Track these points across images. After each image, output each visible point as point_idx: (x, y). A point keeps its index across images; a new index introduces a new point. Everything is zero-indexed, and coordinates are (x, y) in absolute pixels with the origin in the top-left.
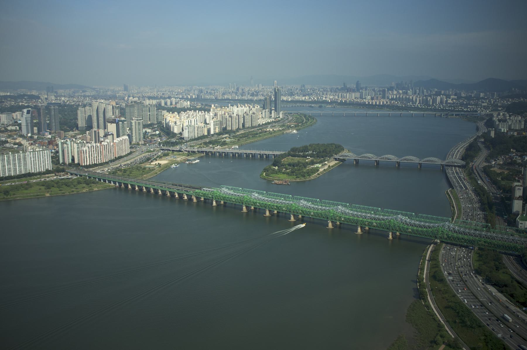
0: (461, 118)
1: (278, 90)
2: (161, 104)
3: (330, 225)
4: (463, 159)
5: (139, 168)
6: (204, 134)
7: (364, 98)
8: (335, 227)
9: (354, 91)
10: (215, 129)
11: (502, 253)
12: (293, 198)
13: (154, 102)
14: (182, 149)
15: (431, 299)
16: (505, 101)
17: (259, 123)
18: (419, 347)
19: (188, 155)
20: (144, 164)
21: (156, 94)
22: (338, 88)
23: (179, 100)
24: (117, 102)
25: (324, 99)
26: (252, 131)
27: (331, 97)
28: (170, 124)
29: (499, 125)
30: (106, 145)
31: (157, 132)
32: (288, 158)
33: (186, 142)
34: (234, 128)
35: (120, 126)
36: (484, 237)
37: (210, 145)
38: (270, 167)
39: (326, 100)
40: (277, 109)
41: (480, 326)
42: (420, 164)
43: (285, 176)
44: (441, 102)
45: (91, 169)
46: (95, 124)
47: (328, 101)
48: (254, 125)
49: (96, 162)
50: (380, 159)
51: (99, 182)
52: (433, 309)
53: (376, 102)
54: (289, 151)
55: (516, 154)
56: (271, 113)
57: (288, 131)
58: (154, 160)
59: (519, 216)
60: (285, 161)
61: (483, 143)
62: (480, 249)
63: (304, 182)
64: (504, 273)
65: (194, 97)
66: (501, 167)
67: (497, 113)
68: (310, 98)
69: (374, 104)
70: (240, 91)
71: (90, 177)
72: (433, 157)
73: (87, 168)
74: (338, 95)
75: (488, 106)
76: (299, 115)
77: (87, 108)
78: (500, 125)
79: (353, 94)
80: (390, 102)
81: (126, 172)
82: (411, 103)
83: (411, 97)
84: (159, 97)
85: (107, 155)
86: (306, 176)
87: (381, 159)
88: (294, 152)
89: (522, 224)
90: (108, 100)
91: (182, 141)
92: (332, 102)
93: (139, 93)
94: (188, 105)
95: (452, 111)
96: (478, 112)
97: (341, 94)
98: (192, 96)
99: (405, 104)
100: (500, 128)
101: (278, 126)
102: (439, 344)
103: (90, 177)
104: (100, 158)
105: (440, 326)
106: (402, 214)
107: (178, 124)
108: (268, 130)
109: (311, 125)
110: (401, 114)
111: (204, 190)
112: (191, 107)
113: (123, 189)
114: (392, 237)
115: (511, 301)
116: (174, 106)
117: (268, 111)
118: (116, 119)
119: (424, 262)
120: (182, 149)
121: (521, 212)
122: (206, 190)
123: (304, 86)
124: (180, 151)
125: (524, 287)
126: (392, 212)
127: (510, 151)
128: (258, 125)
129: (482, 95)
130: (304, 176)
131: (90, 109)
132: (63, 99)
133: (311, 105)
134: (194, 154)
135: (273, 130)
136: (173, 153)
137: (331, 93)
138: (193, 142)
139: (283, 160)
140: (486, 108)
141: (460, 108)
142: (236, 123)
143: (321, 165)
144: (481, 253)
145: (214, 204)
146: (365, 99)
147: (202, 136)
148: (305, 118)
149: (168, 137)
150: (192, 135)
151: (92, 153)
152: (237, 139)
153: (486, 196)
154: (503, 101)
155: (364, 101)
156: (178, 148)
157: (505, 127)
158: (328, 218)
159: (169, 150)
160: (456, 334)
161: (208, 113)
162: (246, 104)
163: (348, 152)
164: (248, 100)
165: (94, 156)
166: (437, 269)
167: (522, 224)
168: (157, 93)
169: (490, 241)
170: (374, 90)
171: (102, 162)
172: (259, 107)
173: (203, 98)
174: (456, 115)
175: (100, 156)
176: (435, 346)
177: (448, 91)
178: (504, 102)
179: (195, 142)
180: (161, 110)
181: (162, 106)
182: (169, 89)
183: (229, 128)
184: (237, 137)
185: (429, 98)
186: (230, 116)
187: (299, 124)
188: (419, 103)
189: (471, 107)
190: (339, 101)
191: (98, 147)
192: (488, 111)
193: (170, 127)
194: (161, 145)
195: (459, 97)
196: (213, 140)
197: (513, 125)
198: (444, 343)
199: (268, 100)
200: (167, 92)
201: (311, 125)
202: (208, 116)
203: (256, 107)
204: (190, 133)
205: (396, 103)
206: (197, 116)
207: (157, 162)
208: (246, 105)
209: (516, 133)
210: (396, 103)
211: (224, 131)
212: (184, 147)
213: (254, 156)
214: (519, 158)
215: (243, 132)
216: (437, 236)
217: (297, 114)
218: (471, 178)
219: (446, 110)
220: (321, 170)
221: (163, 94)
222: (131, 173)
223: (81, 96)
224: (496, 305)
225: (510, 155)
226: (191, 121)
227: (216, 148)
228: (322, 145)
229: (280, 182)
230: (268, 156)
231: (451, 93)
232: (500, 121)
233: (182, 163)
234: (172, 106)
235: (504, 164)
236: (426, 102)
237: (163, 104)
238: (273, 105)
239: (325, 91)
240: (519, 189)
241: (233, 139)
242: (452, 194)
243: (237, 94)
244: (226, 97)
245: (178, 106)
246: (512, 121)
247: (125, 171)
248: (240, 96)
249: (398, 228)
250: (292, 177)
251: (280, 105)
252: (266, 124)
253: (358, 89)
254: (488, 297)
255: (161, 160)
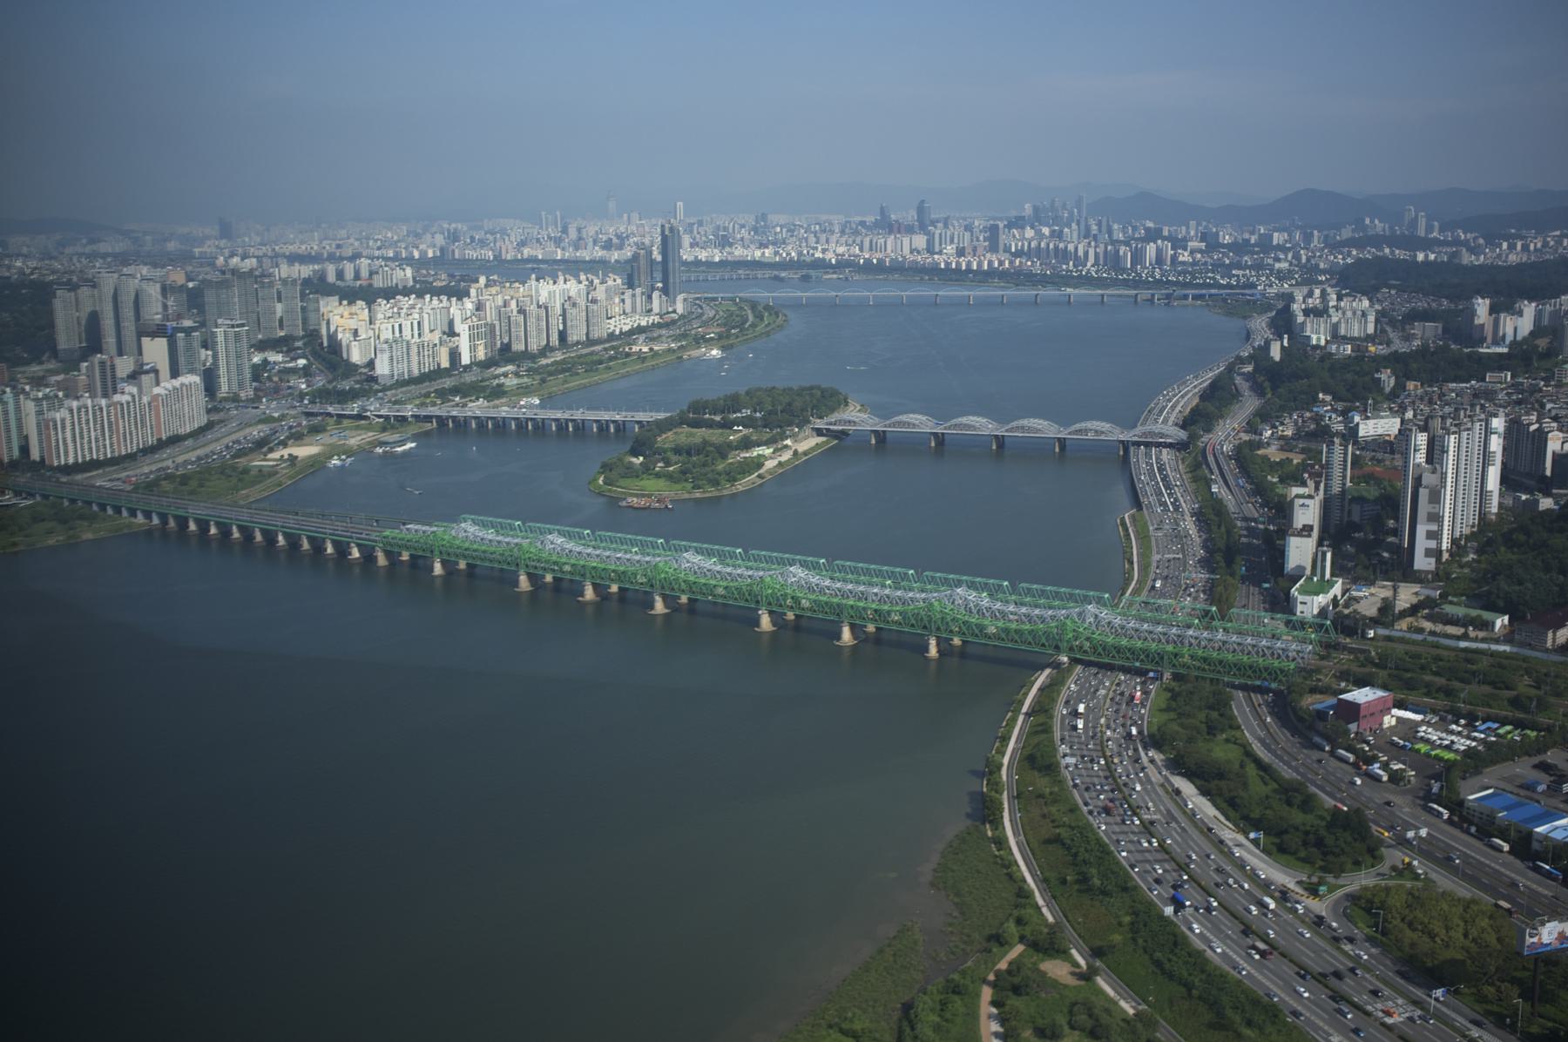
0: (1208, 305)
1: (671, 229)
2: (325, 276)
3: (766, 622)
4: (1184, 426)
5: (228, 472)
6: (439, 365)
7: (937, 250)
8: (779, 629)
9: (910, 230)
10: (473, 349)
11: (1234, 687)
12: (667, 547)
13: (306, 271)
14: (366, 411)
15: (1011, 821)
16: (1340, 257)
17: (612, 328)
18: (953, 953)
19: (384, 430)
20: (247, 458)
21: (316, 248)
22: (865, 222)
23: (383, 263)
24: (191, 272)
25: (818, 255)
26: (586, 355)
27: (841, 250)
28: (340, 336)
29: (1303, 323)
30: (128, 403)
31: (302, 362)
32: (679, 430)
33: (385, 389)
34: (534, 347)
35: (181, 344)
36: (1279, 657)
37: (456, 396)
38: (620, 460)
39: (824, 259)
40: (671, 286)
41: (1125, 889)
42: (1062, 441)
43: (661, 483)
44: (1160, 260)
45: (79, 477)
46: (110, 340)
47: (830, 260)
48: (595, 335)
49: (98, 455)
50: (1007, 431)
51: (101, 513)
52: (1011, 849)
53: (969, 264)
54: (682, 411)
55: (1332, 409)
56: (650, 297)
57: (695, 353)
58: (279, 444)
59: (1302, 581)
60: (667, 439)
61: (1248, 377)
62: (1177, 677)
63: (718, 498)
64: (1227, 741)
65: (430, 254)
66: (1286, 444)
67: (1305, 290)
68: (776, 253)
69: (964, 268)
70: (573, 234)
71: (73, 501)
72: (1098, 420)
73: (69, 474)
74: (862, 242)
75: (1289, 270)
76: (737, 304)
77: (85, 292)
78: (1309, 325)
79: (906, 241)
80: (1011, 263)
81: (185, 484)
82: (1071, 263)
83: (1071, 247)
84: (325, 255)
85: (131, 434)
86: (723, 482)
87: (1011, 430)
88: (695, 415)
89: (1305, 603)
90: (163, 266)
91: (371, 388)
92: (842, 265)
93: (265, 245)
94: (407, 280)
95: (1185, 285)
96: (1259, 288)
97: (871, 241)
98: (426, 252)
99: (1054, 268)
100: (1308, 334)
101: (668, 337)
102: (1007, 943)
103: (73, 501)
104: (108, 442)
105: (1023, 894)
106: (972, 586)
107: (363, 336)
108: (635, 349)
109: (768, 334)
110: (1036, 295)
111: (408, 529)
112: (418, 286)
113: (174, 536)
114: (938, 652)
115: (1228, 818)
116: (364, 283)
117: (643, 294)
118: (168, 324)
119: (1014, 720)
120: (366, 411)
121: (1308, 572)
122: (415, 530)
123: (764, 217)
124: (360, 417)
125: (1271, 778)
126: (1057, 593)
127: (1315, 400)
128: (608, 335)
129: (1278, 238)
130: (716, 483)
131: (93, 296)
132: (18, 264)
133: (776, 273)
134: (402, 426)
135: (651, 349)
136: (339, 423)
137: (841, 237)
138: (404, 389)
139: (664, 436)
140: (1282, 276)
141: (1210, 278)
142: (539, 330)
143: (771, 450)
144: (1177, 689)
145: (438, 569)
146: (940, 253)
147: (434, 371)
148: (753, 312)
149: (331, 377)
150: (402, 369)
151: (81, 429)
152: (538, 377)
153: (1223, 529)
154: (1334, 254)
155: (933, 259)
156: (354, 408)
157: (1322, 329)
158: (758, 602)
159: (329, 415)
160: (1062, 912)
161: (459, 303)
162: (582, 273)
163: (859, 411)
164: (592, 262)
165: (90, 437)
166: (1043, 736)
167: (1305, 603)
168: (321, 243)
169: (1205, 655)
170: (969, 228)
171: (117, 454)
172: (619, 281)
173: (457, 256)
174: (1195, 297)
175: (107, 437)
176: (995, 950)
177: (1184, 228)
178: (1335, 257)
179: (409, 388)
180: (316, 296)
181: (329, 284)
182: (361, 232)
183: (518, 347)
184: (539, 374)
185: (1122, 249)
186: (521, 311)
187: (733, 331)
188: (1096, 263)
189: (1241, 273)
190: (862, 261)
191: (101, 409)
192: (1286, 286)
193: (341, 345)
194: (306, 402)
195: (1212, 244)
196: (464, 384)
197: (1343, 325)
198: (1022, 939)
199: (642, 262)
200: (352, 240)
201: (768, 334)
202: (460, 311)
203: (610, 283)
204: (395, 362)
205: (1029, 263)
206: (425, 311)
207: (285, 452)
208: (583, 277)
209: (1349, 346)
210: (1029, 263)
211: (505, 354)
212: (373, 407)
213: (581, 427)
214: (1339, 419)
215: (558, 359)
216: (1060, 644)
217: (733, 300)
218: (1195, 480)
219: (1168, 282)
220: (770, 464)
221: (339, 246)
222: (202, 486)
223: (80, 255)
224: (1183, 829)
225: (1315, 409)
226: (400, 325)
227: (471, 405)
228: (784, 390)
229: (643, 502)
230: (621, 427)
231: (1192, 233)
232: (1307, 312)
233: (364, 452)
234: (358, 283)
235: (1297, 436)
236: (1114, 261)
237: (331, 278)
238: (658, 275)
239: (824, 231)
240: (1303, 505)
241: (526, 380)
242: (1135, 526)
243: (562, 245)
244: (527, 252)
245: (378, 282)
246: (1344, 313)
247: (185, 479)
248: (571, 249)
249: (683, 586)
250: (678, 486)
251: (677, 275)
252: (632, 332)
253: (923, 224)
254: (1169, 811)
255: (299, 446)
